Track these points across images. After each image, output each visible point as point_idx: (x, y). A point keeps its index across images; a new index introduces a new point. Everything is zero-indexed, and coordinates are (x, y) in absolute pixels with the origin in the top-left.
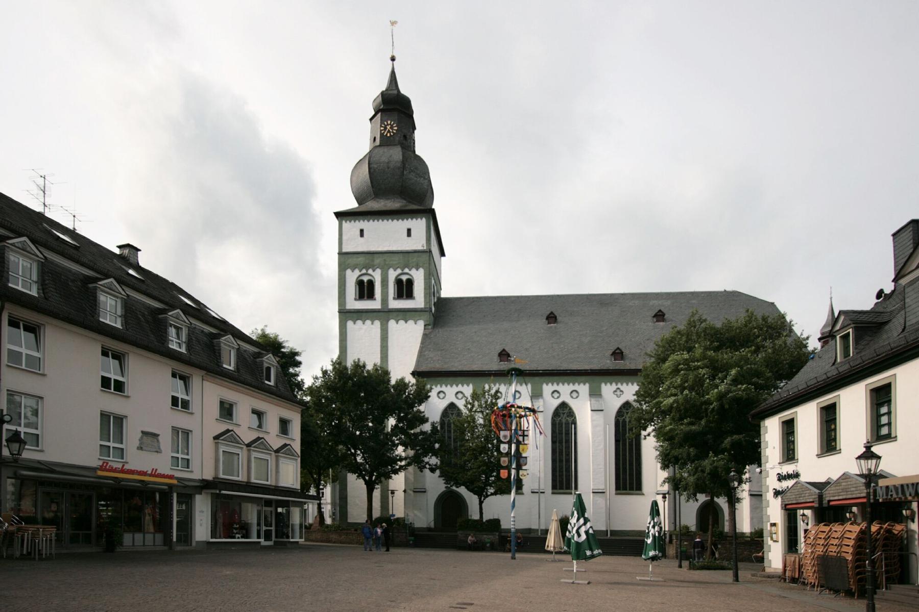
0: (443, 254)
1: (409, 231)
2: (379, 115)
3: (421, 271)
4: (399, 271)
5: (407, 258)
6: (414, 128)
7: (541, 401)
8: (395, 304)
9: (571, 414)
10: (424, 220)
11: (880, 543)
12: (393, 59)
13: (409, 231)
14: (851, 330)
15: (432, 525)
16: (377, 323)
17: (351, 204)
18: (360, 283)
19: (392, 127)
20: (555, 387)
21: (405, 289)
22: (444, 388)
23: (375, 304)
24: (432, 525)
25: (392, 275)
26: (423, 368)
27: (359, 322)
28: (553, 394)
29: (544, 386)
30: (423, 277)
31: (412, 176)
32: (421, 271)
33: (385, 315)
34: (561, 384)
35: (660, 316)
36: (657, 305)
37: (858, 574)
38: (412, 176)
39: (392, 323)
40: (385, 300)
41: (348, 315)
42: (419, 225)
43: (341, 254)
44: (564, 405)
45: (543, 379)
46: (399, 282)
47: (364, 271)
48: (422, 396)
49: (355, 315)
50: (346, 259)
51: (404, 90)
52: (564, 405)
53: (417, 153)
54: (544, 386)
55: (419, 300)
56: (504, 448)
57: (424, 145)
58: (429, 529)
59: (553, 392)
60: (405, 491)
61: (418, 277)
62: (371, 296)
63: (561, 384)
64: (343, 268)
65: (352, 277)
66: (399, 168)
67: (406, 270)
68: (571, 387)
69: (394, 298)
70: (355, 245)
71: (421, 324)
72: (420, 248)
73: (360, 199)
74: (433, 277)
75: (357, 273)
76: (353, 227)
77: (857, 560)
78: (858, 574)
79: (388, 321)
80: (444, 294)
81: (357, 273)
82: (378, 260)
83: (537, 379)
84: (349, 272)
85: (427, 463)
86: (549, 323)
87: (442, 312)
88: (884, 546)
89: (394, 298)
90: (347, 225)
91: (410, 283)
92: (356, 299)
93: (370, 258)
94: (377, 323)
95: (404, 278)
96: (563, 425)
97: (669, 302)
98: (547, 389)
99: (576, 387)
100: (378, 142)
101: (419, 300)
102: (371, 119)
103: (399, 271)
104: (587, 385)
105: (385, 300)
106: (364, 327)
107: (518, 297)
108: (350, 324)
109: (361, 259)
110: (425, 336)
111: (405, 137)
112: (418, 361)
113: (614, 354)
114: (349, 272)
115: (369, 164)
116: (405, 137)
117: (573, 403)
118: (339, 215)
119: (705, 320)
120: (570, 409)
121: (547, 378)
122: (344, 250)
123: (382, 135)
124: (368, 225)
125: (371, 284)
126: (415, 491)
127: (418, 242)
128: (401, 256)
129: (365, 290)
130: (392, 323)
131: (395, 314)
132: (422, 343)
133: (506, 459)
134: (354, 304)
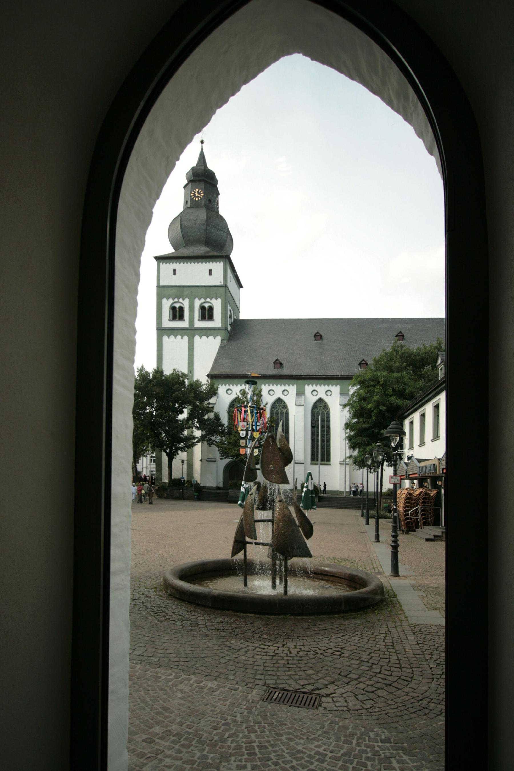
0: (240, 286)
1: (210, 271)
2: (190, 184)
3: (219, 301)
4: (203, 300)
5: (208, 291)
6: (218, 194)
7: (303, 397)
8: (199, 324)
9: (326, 406)
10: (222, 263)
11: (421, 501)
12: (202, 142)
13: (210, 271)
14: (443, 366)
15: (221, 485)
16: (186, 338)
17: (169, 250)
18: (173, 309)
19: (199, 193)
20: (314, 387)
21: (207, 313)
22: (231, 387)
23: (184, 324)
24: (221, 485)
25: (198, 303)
26: (214, 373)
27: (172, 337)
28: (315, 392)
29: (306, 386)
30: (220, 305)
31: (213, 230)
32: (219, 301)
33: (191, 332)
34: (318, 386)
35: (400, 336)
36: (400, 327)
37: (406, 519)
38: (213, 230)
39: (197, 338)
40: (191, 321)
41: (164, 331)
42: (218, 267)
43: (159, 287)
44: (320, 400)
45: (305, 381)
46: (203, 308)
47: (176, 300)
48: (213, 392)
49: (169, 332)
50: (163, 291)
51: (211, 166)
52: (320, 400)
53: (220, 213)
54: (306, 386)
55: (217, 322)
56: (243, 434)
57: (225, 207)
58: (218, 488)
59: (312, 391)
60: (201, 460)
61: (217, 304)
62: (182, 318)
63: (318, 386)
64: (160, 297)
65: (167, 304)
66: (203, 225)
67: (208, 300)
68: (326, 388)
69: (199, 320)
70: (169, 280)
71: (219, 339)
72: (218, 283)
73: (175, 246)
74: (231, 303)
75: (171, 301)
76: (168, 267)
77: (405, 511)
78: (406, 519)
79: (194, 336)
80: (242, 316)
81: (171, 301)
82: (187, 292)
83: (301, 381)
84: (164, 300)
85: (214, 441)
86: (315, 340)
87: (237, 330)
88: (423, 502)
89: (199, 320)
90: (163, 266)
91: (211, 309)
92: (169, 320)
93: (180, 291)
94: (186, 338)
95: (207, 305)
96: (320, 414)
97: (410, 326)
98: (308, 389)
99: (330, 388)
100: (189, 204)
101: (217, 322)
102: (184, 187)
103: (203, 300)
104: (338, 387)
105: (191, 321)
106: (176, 340)
107: (296, 320)
108: (165, 338)
109: (174, 290)
110: (221, 348)
111: (210, 201)
112: (213, 367)
113: (360, 364)
114: (164, 300)
115: (181, 221)
116: (210, 201)
117: (326, 399)
118: (158, 258)
119: (404, 346)
120: (326, 403)
121: (308, 381)
122: (161, 284)
123: (192, 199)
124: (179, 266)
125: (181, 309)
126: (206, 460)
127: (217, 279)
128: (204, 289)
129: (177, 313)
130: (197, 338)
131: (199, 331)
132: (218, 353)
133: (244, 441)
134: (167, 323)
